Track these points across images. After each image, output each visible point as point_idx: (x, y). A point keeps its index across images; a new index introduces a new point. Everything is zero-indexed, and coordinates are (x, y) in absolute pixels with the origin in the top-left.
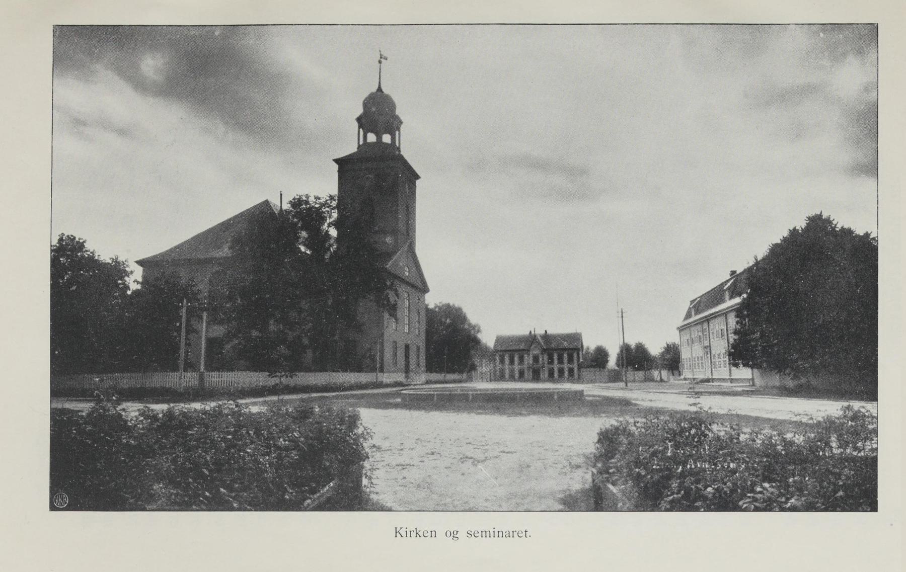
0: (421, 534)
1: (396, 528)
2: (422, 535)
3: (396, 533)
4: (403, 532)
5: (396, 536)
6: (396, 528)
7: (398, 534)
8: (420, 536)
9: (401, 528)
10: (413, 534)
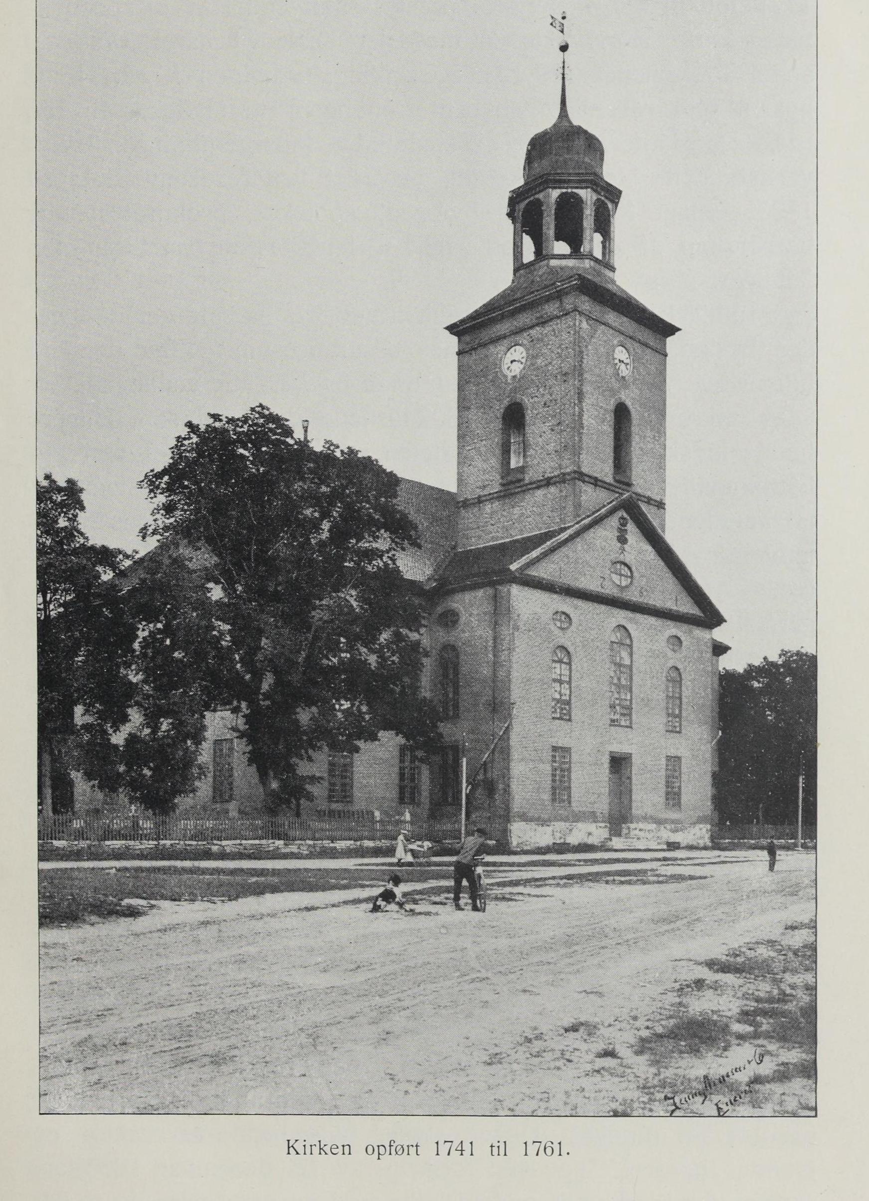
0: (327, 1149)
1: (288, 1141)
2: (328, 1151)
3: (289, 1148)
4: (299, 1147)
5: (289, 1153)
6: (288, 1141)
7: (291, 1149)
8: (326, 1154)
9: (296, 1141)
10: (316, 1150)
